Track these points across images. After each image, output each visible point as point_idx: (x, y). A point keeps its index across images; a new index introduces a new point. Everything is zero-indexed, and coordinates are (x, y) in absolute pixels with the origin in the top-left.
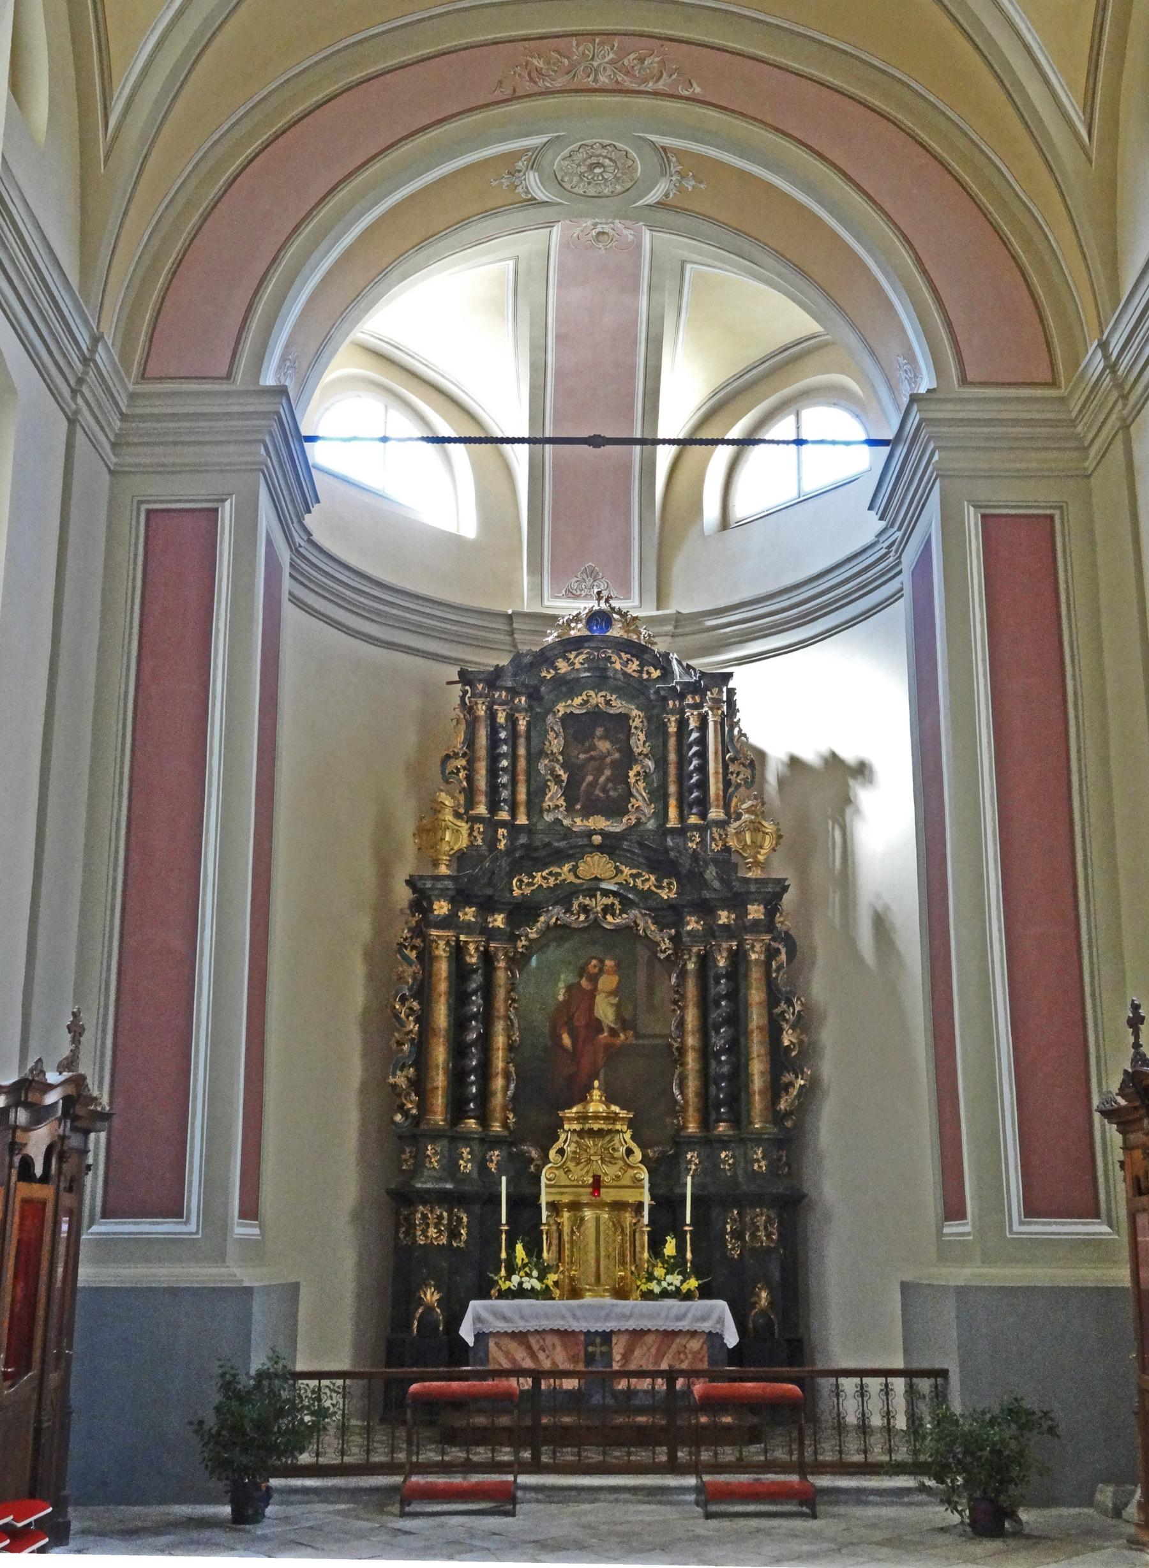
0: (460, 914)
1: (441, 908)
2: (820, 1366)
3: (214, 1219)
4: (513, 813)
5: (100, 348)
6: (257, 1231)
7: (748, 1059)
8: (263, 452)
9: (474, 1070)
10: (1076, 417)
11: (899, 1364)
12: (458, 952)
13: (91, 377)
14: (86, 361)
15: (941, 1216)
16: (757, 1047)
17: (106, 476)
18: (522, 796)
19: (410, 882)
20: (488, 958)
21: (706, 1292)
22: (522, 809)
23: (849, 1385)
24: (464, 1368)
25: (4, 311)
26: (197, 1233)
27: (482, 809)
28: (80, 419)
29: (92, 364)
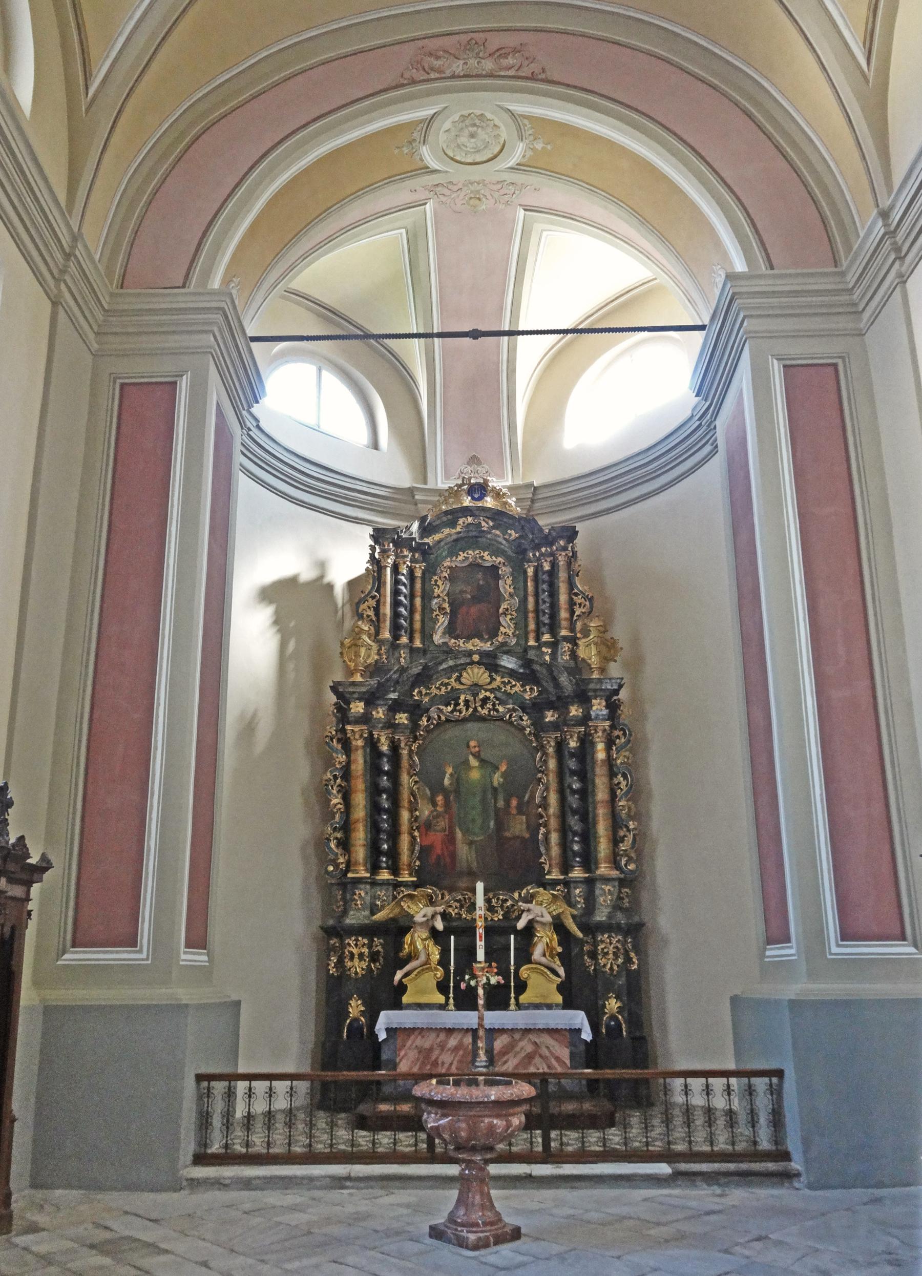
0: (374, 713)
1: (358, 708)
2: (661, 1067)
3: (162, 944)
4: (411, 639)
5: (80, 246)
6: (205, 958)
7: (595, 823)
8: (212, 339)
9: (386, 854)
10: (854, 287)
11: (731, 1066)
12: (372, 743)
13: (73, 268)
14: (67, 256)
15: (762, 938)
16: (602, 812)
17: (89, 358)
18: (417, 625)
19: (334, 689)
20: (395, 747)
21: (568, 1004)
22: (417, 636)
23: (678, 1082)
24: (380, 1072)
25: (9, 226)
26: (147, 959)
27: (386, 634)
28: (62, 300)
29: (72, 258)
